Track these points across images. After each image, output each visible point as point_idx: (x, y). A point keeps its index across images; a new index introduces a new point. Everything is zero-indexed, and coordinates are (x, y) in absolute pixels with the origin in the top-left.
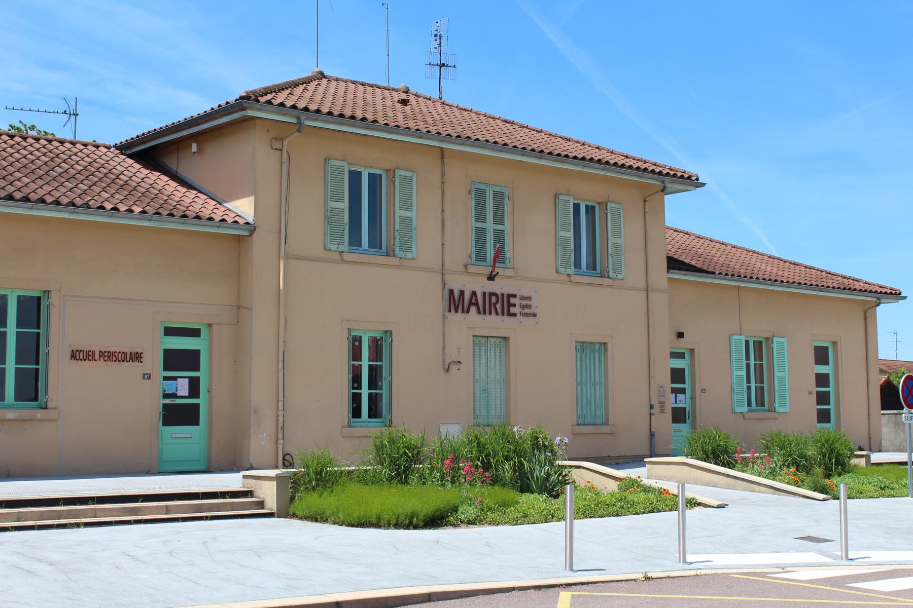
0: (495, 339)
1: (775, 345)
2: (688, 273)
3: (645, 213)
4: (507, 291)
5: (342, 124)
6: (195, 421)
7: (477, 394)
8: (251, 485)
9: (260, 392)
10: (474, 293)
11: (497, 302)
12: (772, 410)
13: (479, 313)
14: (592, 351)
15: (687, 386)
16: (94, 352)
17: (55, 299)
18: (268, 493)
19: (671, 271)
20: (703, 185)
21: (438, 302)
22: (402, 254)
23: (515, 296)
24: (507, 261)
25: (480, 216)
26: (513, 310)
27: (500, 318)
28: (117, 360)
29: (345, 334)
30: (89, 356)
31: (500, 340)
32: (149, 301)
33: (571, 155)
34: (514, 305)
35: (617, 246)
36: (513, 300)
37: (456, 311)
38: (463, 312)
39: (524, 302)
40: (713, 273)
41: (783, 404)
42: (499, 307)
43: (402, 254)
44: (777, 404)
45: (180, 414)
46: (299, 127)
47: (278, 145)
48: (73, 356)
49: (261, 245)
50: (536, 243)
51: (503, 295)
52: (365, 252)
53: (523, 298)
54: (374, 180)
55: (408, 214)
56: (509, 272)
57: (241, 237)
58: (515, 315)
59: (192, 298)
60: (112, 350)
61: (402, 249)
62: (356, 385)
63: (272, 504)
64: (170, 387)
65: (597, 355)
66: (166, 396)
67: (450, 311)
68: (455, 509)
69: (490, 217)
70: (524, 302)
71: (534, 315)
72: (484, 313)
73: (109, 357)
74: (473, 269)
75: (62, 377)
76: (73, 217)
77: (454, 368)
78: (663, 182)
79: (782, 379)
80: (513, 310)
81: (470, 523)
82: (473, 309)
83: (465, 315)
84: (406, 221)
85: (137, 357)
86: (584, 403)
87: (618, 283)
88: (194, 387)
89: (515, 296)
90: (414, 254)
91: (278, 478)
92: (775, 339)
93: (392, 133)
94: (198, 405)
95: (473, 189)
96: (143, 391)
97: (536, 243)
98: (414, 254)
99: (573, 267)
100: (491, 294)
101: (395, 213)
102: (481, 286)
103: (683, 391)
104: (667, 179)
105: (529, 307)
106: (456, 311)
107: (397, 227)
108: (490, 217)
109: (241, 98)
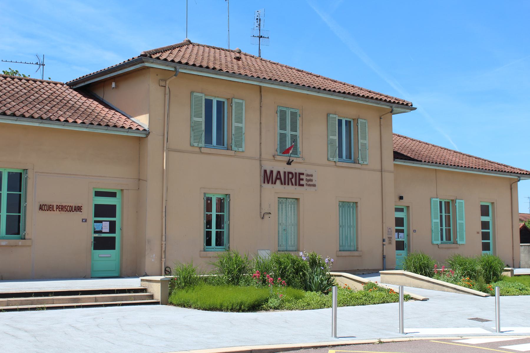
0: (291, 200)
1: (457, 204)
2: (406, 161)
3: (380, 125)
4: (298, 171)
5: (201, 71)
6: (113, 247)
7: (280, 232)
8: (146, 285)
9: (152, 230)
10: (279, 172)
11: (292, 178)
12: (455, 243)
13: (282, 184)
14: (349, 207)
15: (405, 228)
16: (53, 206)
17: (30, 174)
18: (156, 290)
19: (396, 160)
20: (416, 108)
21: (257, 177)
22: (236, 149)
23: (303, 174)
24: (298, 153)
25: (283, 127)
26: (302, 182)
27: (294, 187)
28: (67, 210)
29: (203, 195)
30: (50, 208)
31: (294, 200)
32: (86, 175)
33: (337, 91)
34: (302, 180)
35: (364, 145)
36: (302, 177)
37: (268, 183)
38: (272, 183)
39: (308, 178)
40: (421, 161)
41: (462, 239)
42: (293, 180)
43: (236, 149)
44: (458, 239)
45: (104, 243)
46: (176, 73)
47: (163, 83)
48: (41, 208)
49: (153, 144)
50: (316, 142)
51: (296, 173)
52: (214, 147)
53: (308, 175)
54: (220, 105)
55: (240, 125)
56: (300, 160)
57: (141, 138)
58: (303, 185)
59: (112, 174)
60: (64, 204)
61: (236, 146)
62: (208, 226)
63: (158, 297)
64: (98, 227)
65: (351, 210)
66: (96, 232)
67: (264, 183)
68: (267, 301)
69: (288, 127)
70: (308, 178)
71: (314, 185)
72: (285, 184)
73: (62, 209)
74: (278, 158)
75: (34, 220)
76: (42, 125)
77: (266, 216)
78: (391, 107)
79: (461, 224)
80: (302, 182)
81: (276, 308)
82: (278, 182)
83: (273, 185)
84: (239, 129)
85: (79, 209)
86: (344, 240)
87: (364, 167)
88: (113, 227)
89: (303, 174)
90: (243, 149)
91: (162, 281)
92: (457, 201)
93: (231, 77)
94: (114, 238)
95: (279, 110)
96: (82, 229)
97: (316, 142)
98: (243, 149)
99: (337, 157)
100: (289, 173)
101: (232, 124)
102: (283, 168)
103: (402, 231)
104: (394, 105)
105: (311, 180)
106: (268, 183)
107: (233, 132)
108: (288, 127)
109: (142, 55)
